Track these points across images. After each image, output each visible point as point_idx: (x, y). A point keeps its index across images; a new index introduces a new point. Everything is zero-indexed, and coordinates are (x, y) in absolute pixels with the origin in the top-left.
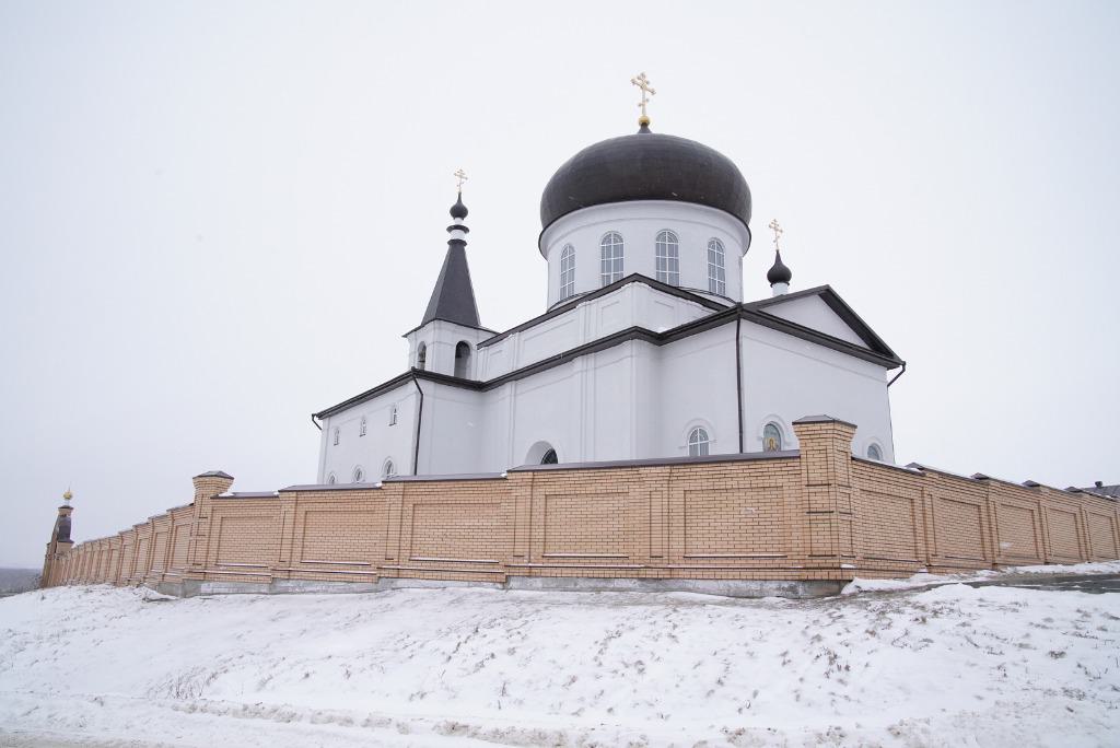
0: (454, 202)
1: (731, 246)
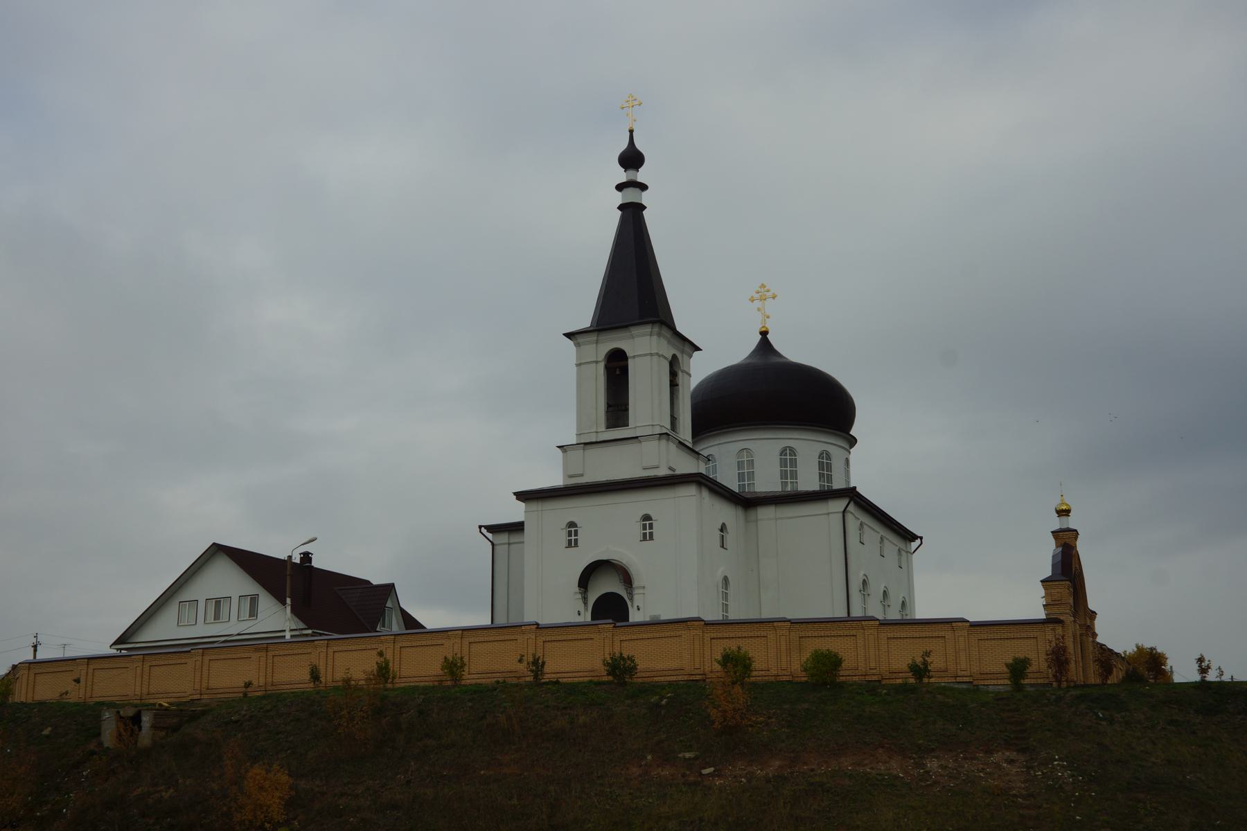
0: (624, 145)
1: (837, 453)
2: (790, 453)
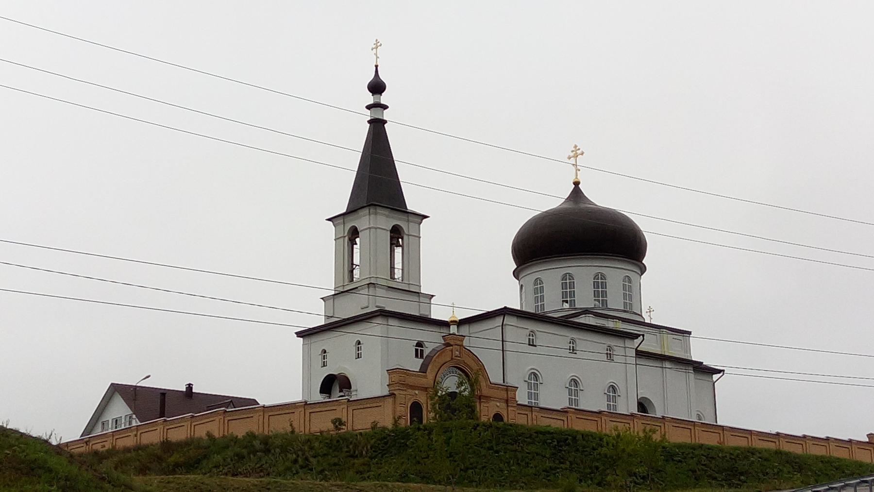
2: (601, 278)
